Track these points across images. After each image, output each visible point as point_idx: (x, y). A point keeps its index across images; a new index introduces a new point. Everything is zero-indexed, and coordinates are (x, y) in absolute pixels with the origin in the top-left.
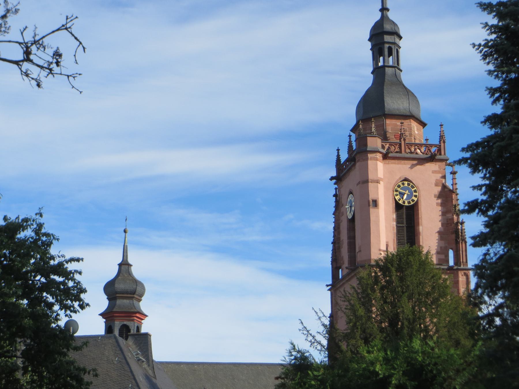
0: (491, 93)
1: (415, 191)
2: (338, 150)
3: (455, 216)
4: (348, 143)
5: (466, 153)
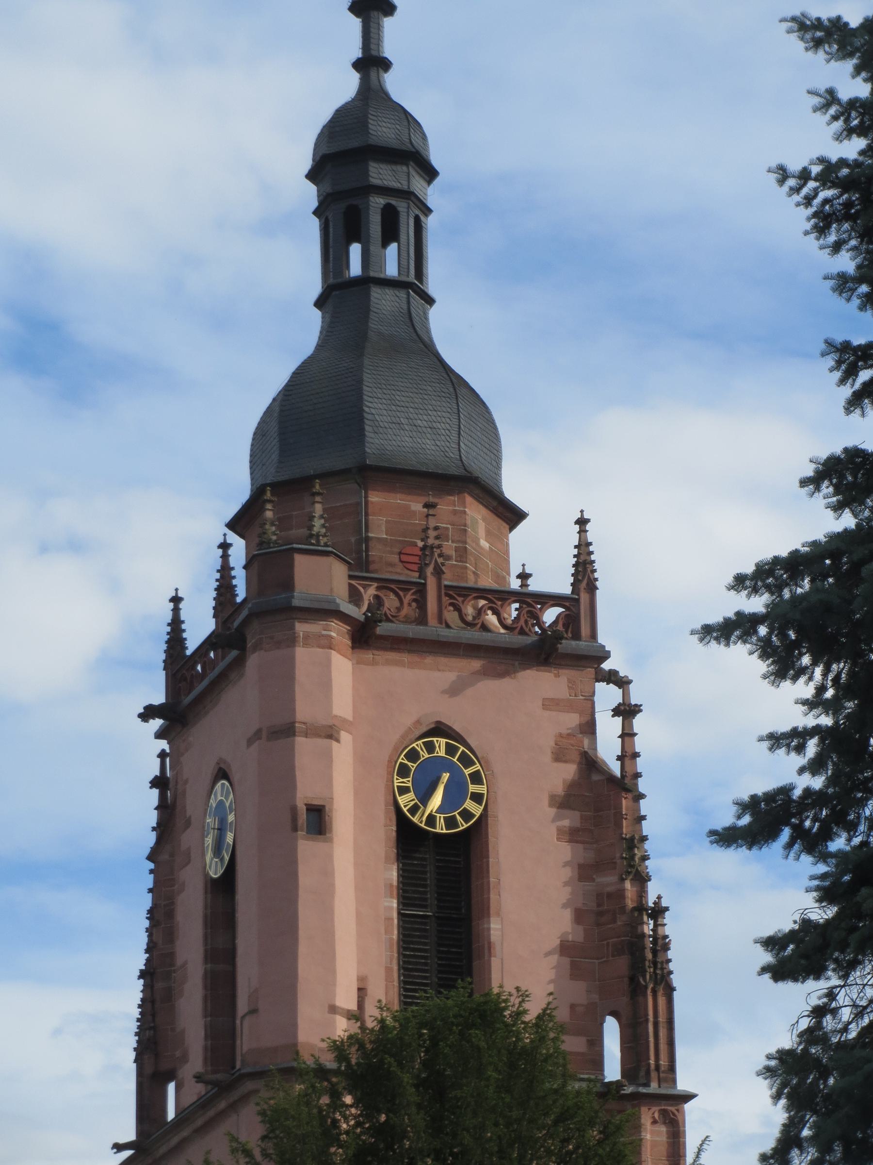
0: (843, 367)
1: (476, 778)
3: (628, 885)
4: (218, 576)
5: (749, 596)
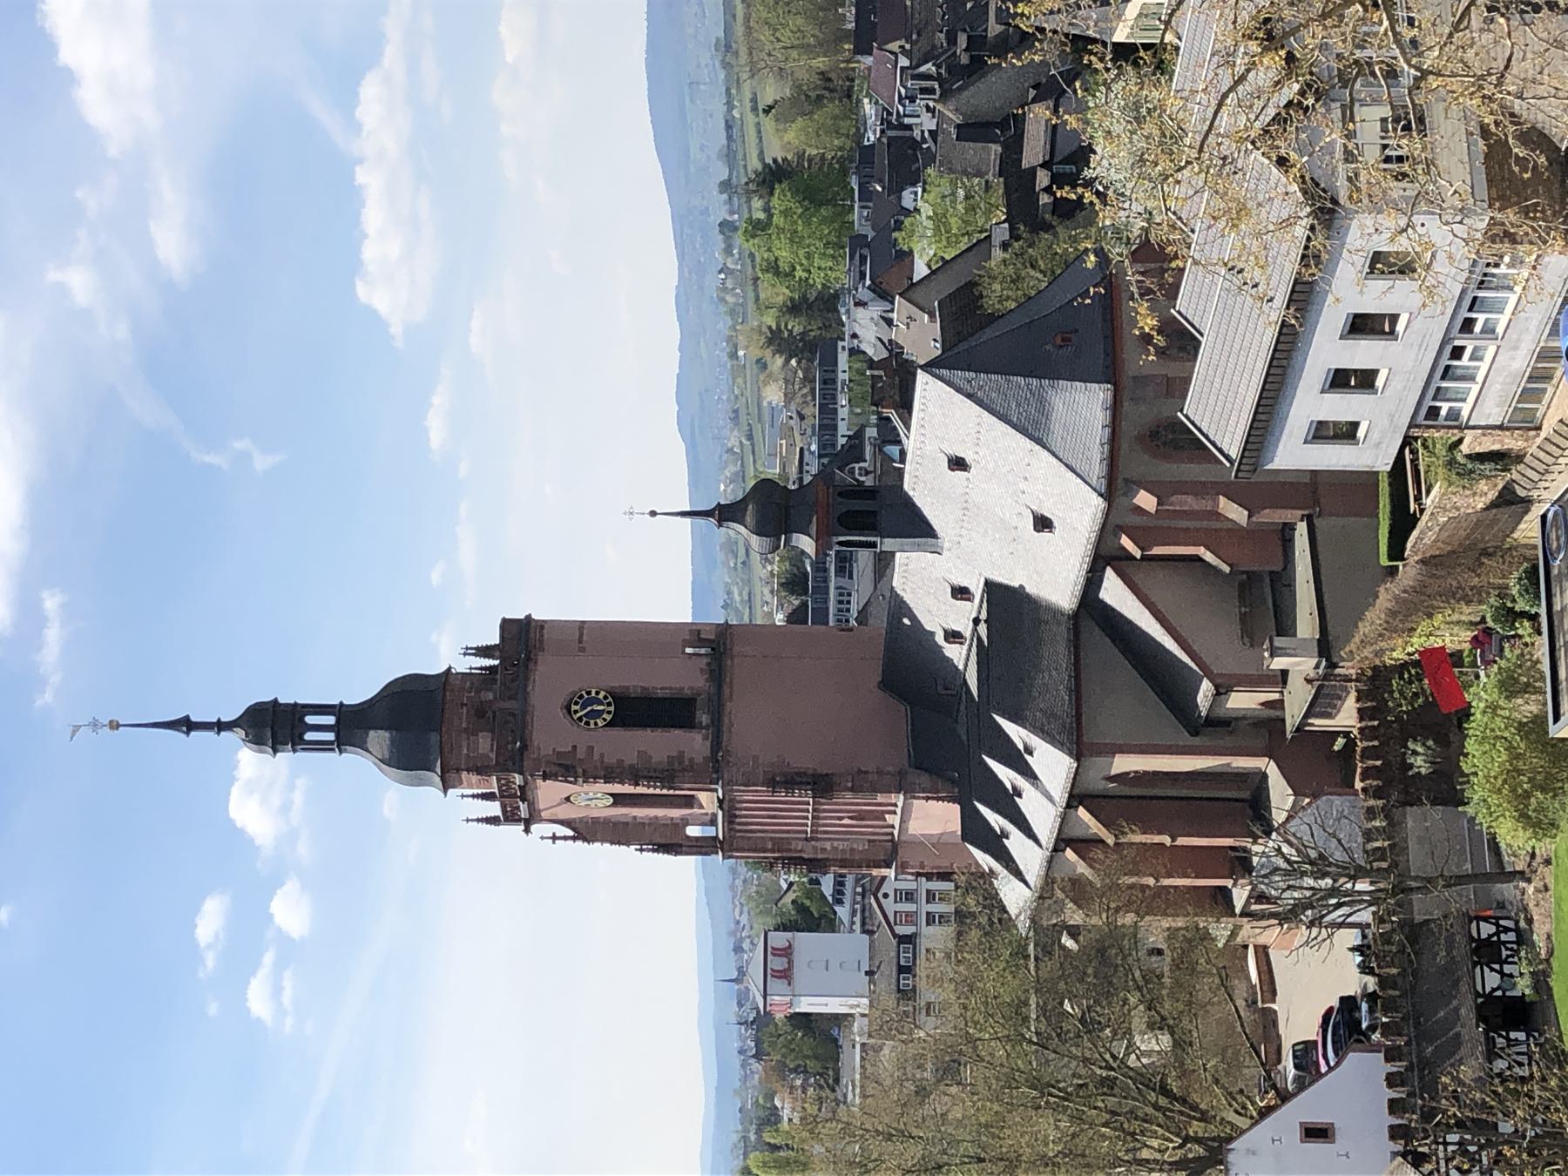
1: (589, 693)
2: (468, 820)
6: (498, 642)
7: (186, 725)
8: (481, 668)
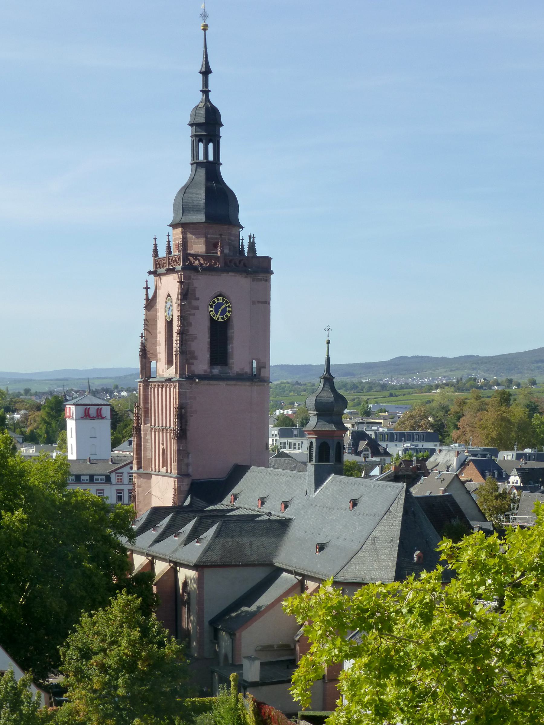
6: (257, 255)
7: (206, 72)
8: (243, 246)
